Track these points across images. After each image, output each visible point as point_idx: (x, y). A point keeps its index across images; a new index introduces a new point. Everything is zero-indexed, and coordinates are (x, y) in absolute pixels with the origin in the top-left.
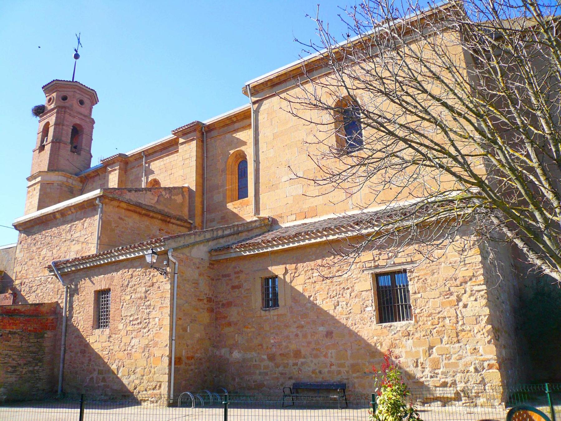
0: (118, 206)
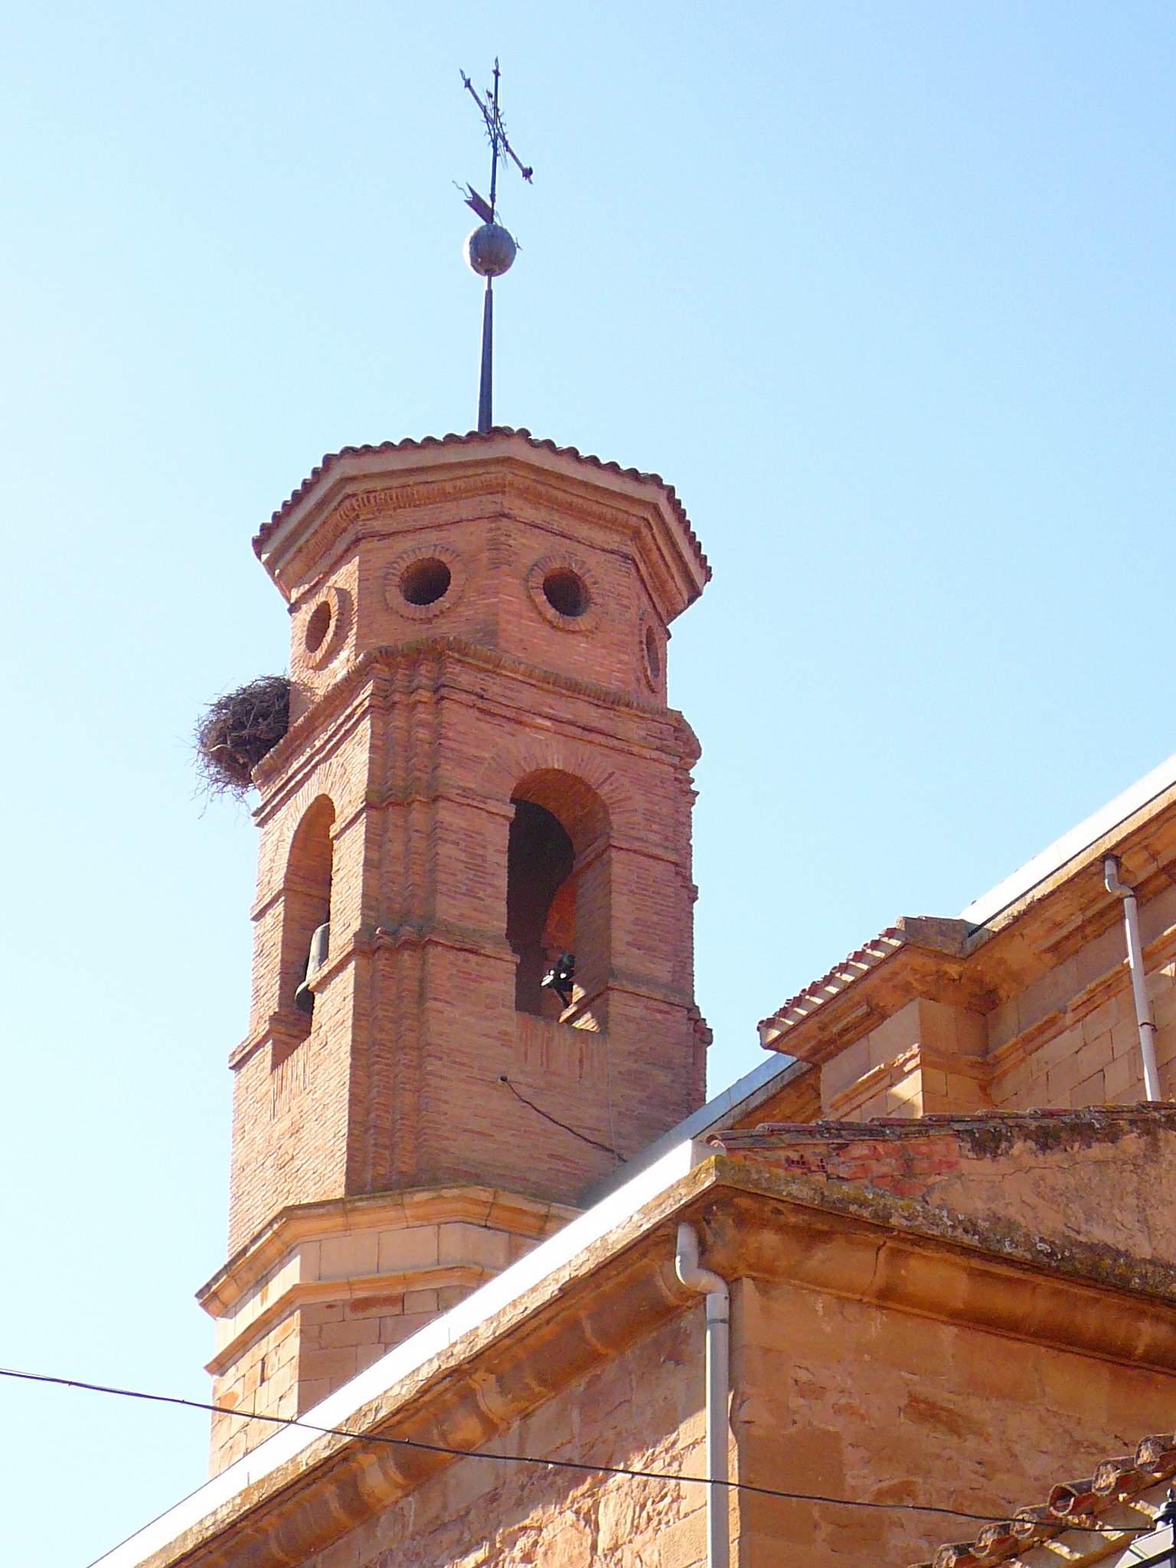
0: (888, 1297)
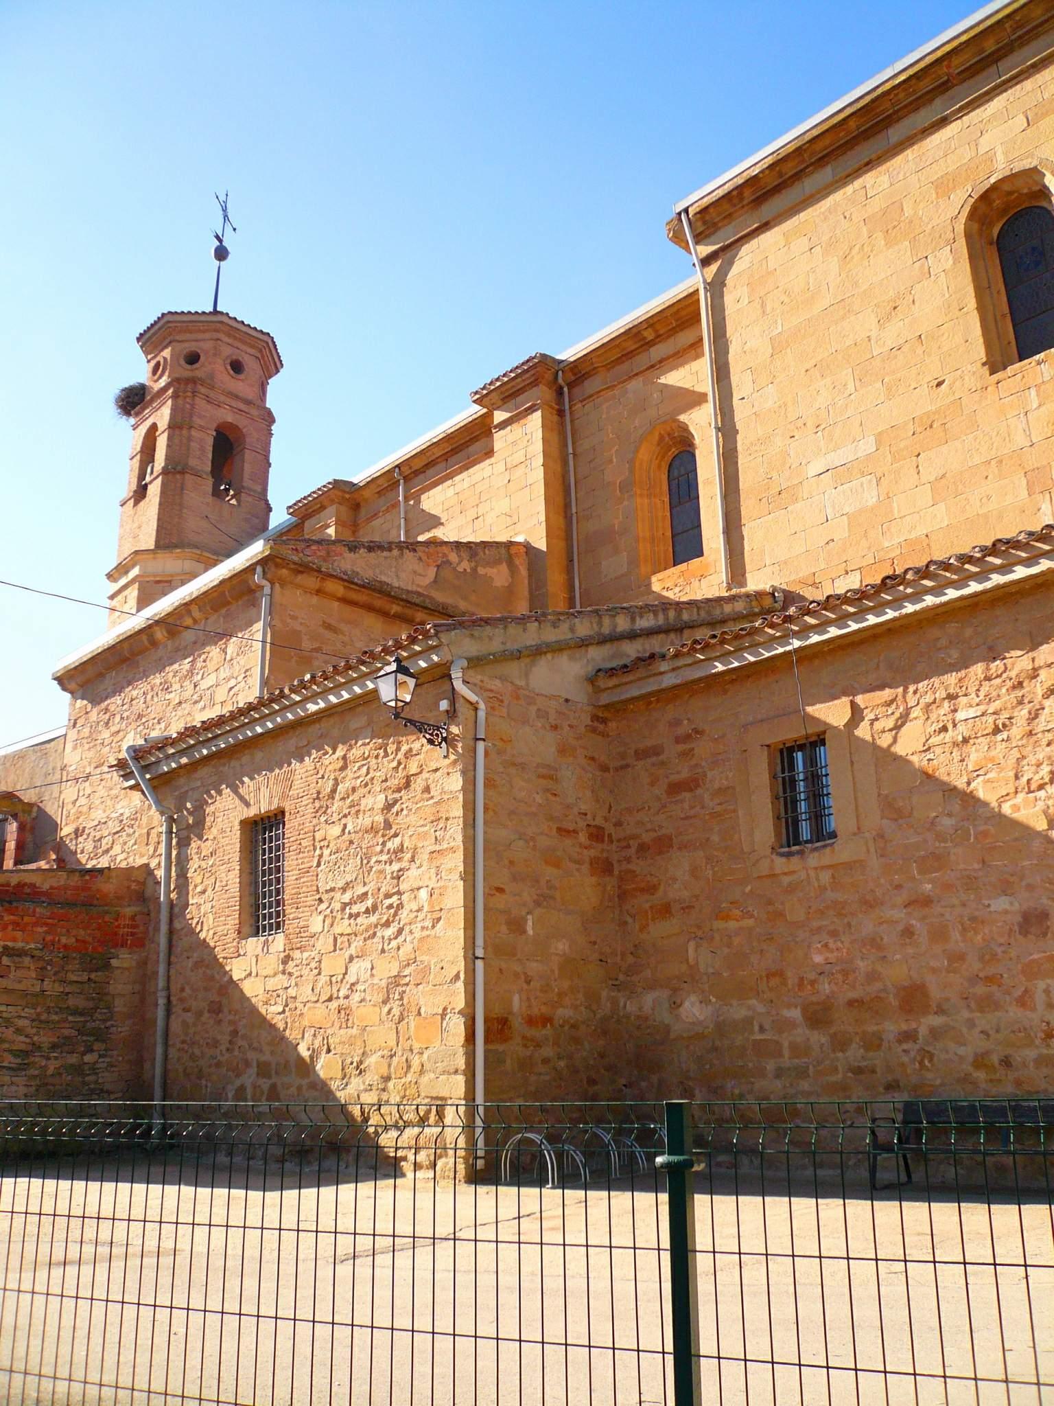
0: (319, 592)
